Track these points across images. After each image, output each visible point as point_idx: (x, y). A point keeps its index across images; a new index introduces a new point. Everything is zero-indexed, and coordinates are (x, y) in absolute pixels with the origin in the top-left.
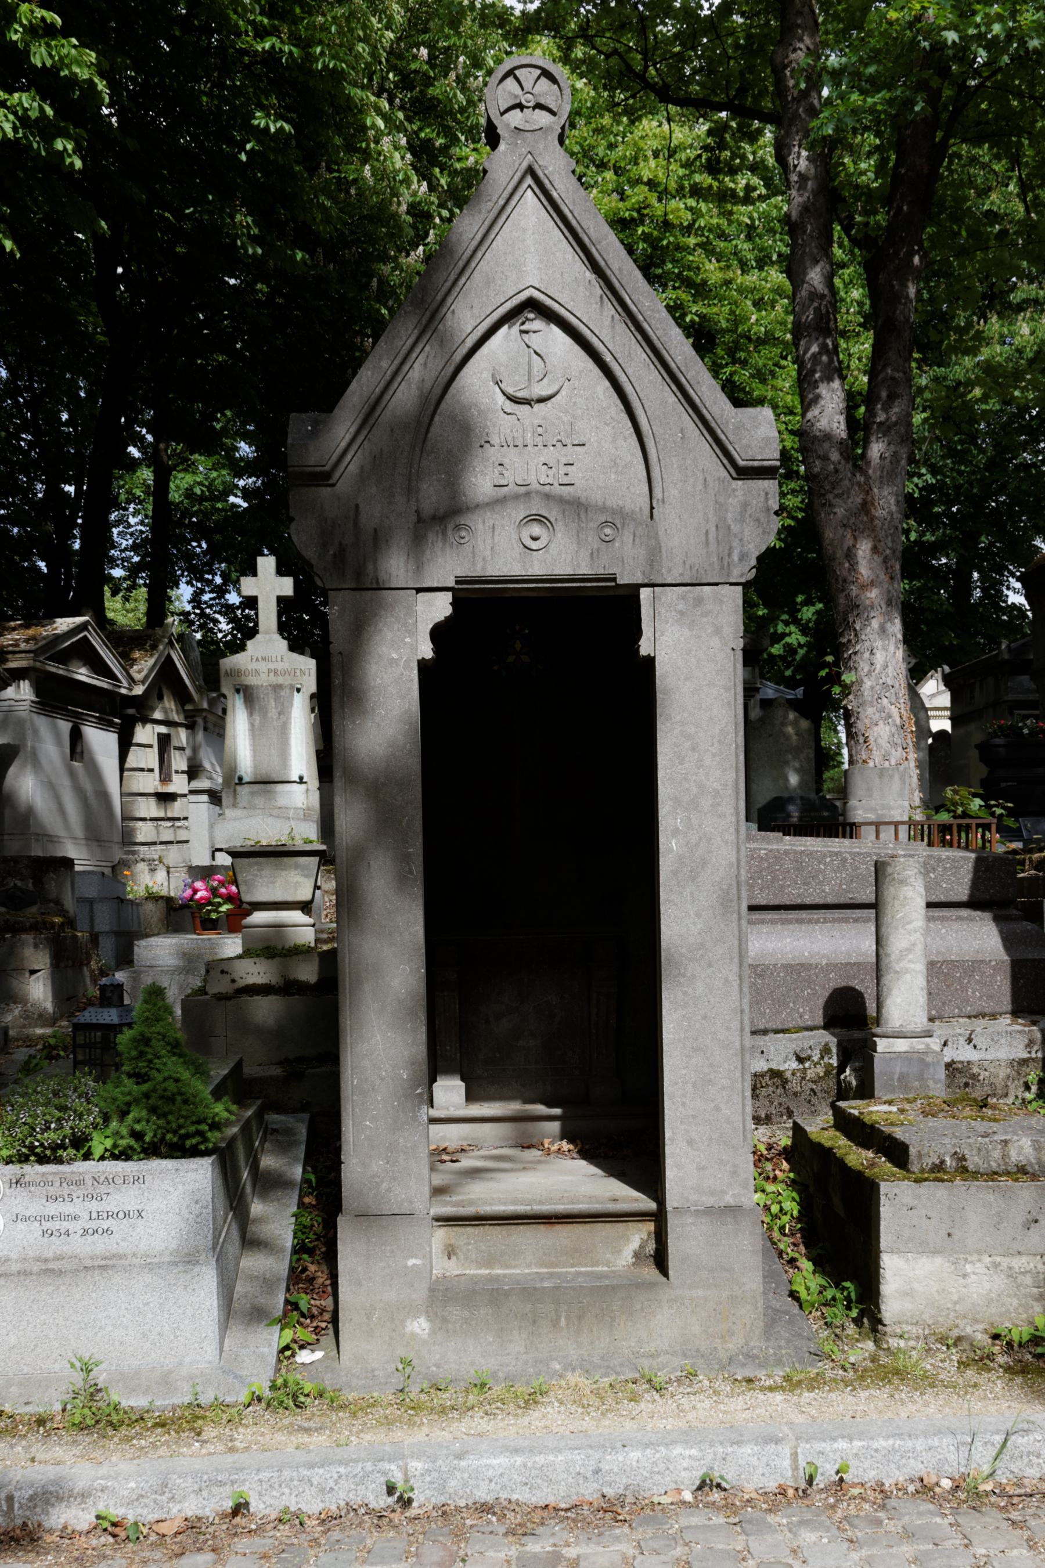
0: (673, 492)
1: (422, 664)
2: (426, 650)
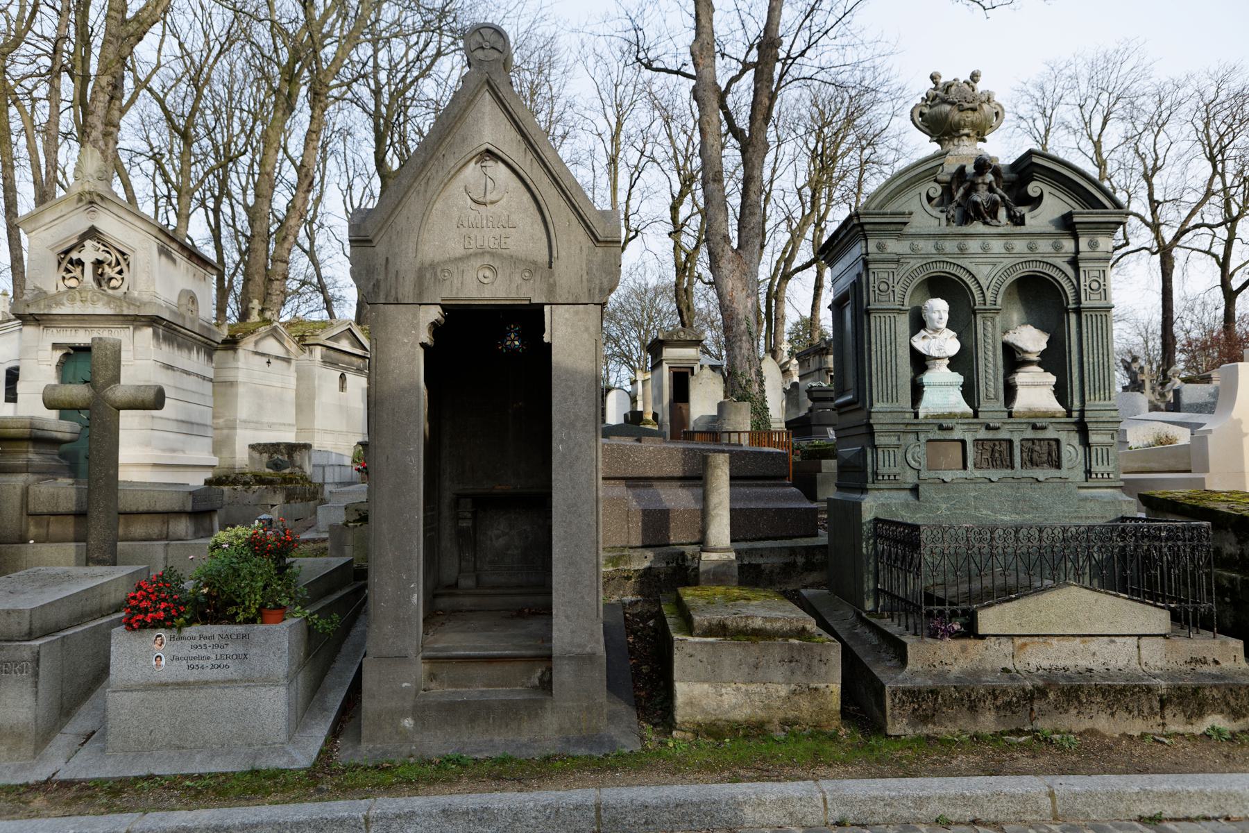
0: (563, 253)
2: (426, 337)
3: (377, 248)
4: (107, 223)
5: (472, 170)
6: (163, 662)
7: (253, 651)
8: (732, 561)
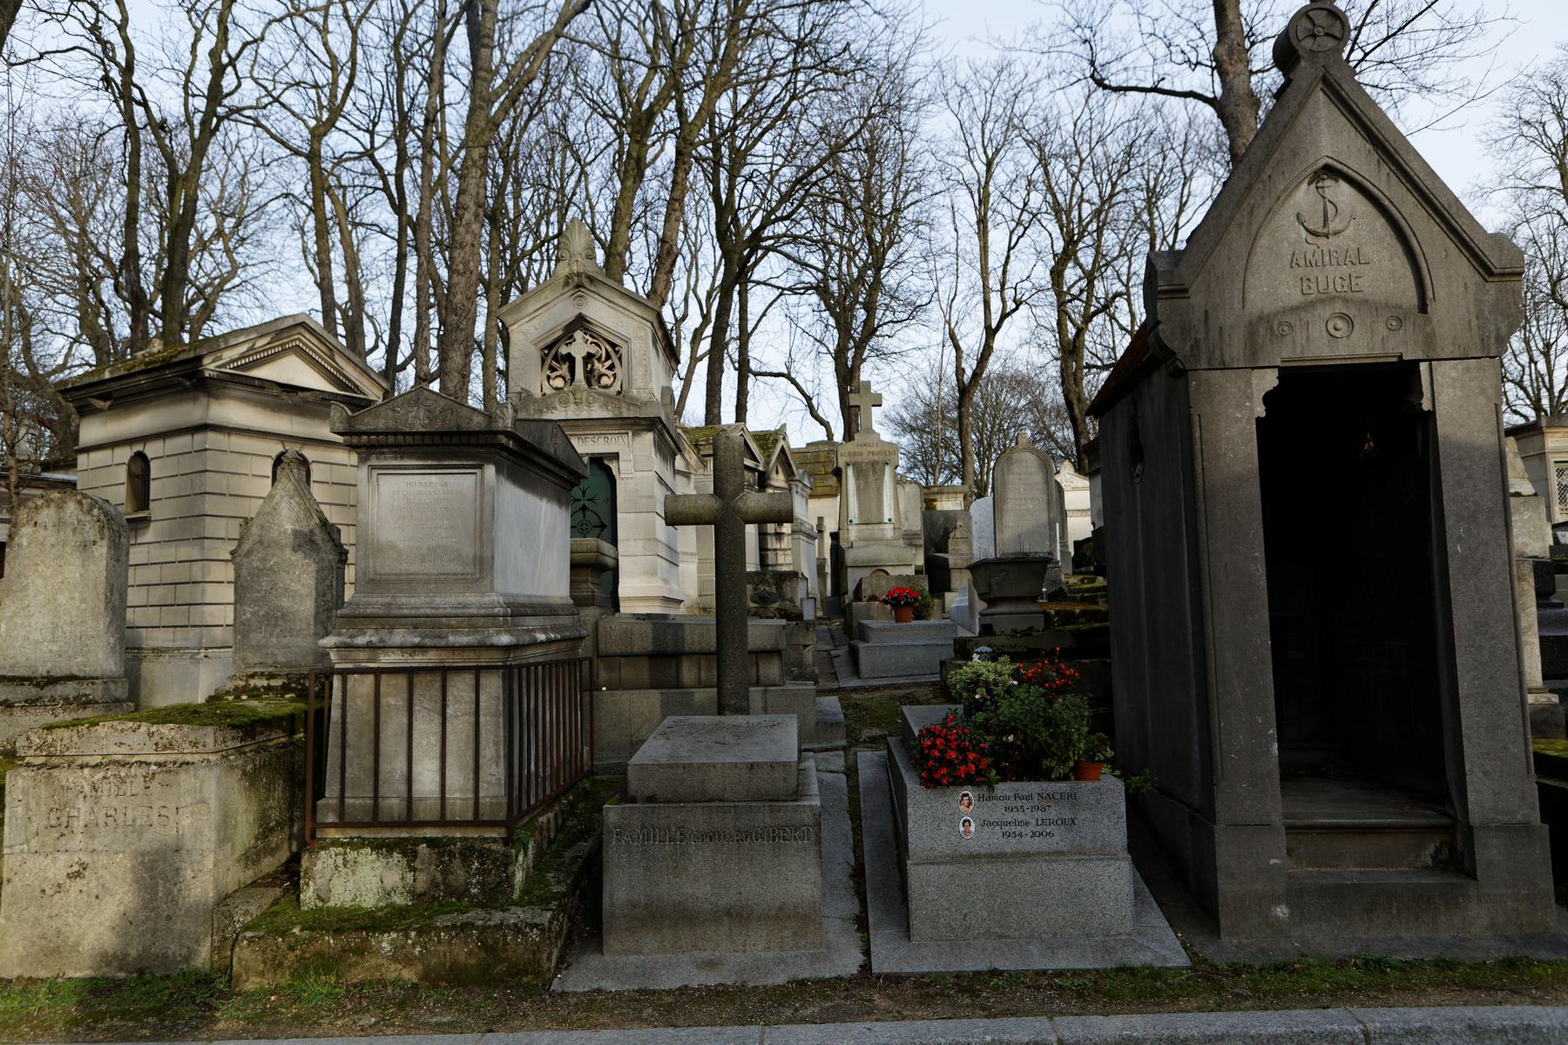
0: (1441, 293)
1: (1259, 420)
2: (1261, 411)
3: (1192, 300)
4: (599, 311)
5: (1304, 196)
6: (972, 829)
7: (1082, 815)
8: (1555, 705)
